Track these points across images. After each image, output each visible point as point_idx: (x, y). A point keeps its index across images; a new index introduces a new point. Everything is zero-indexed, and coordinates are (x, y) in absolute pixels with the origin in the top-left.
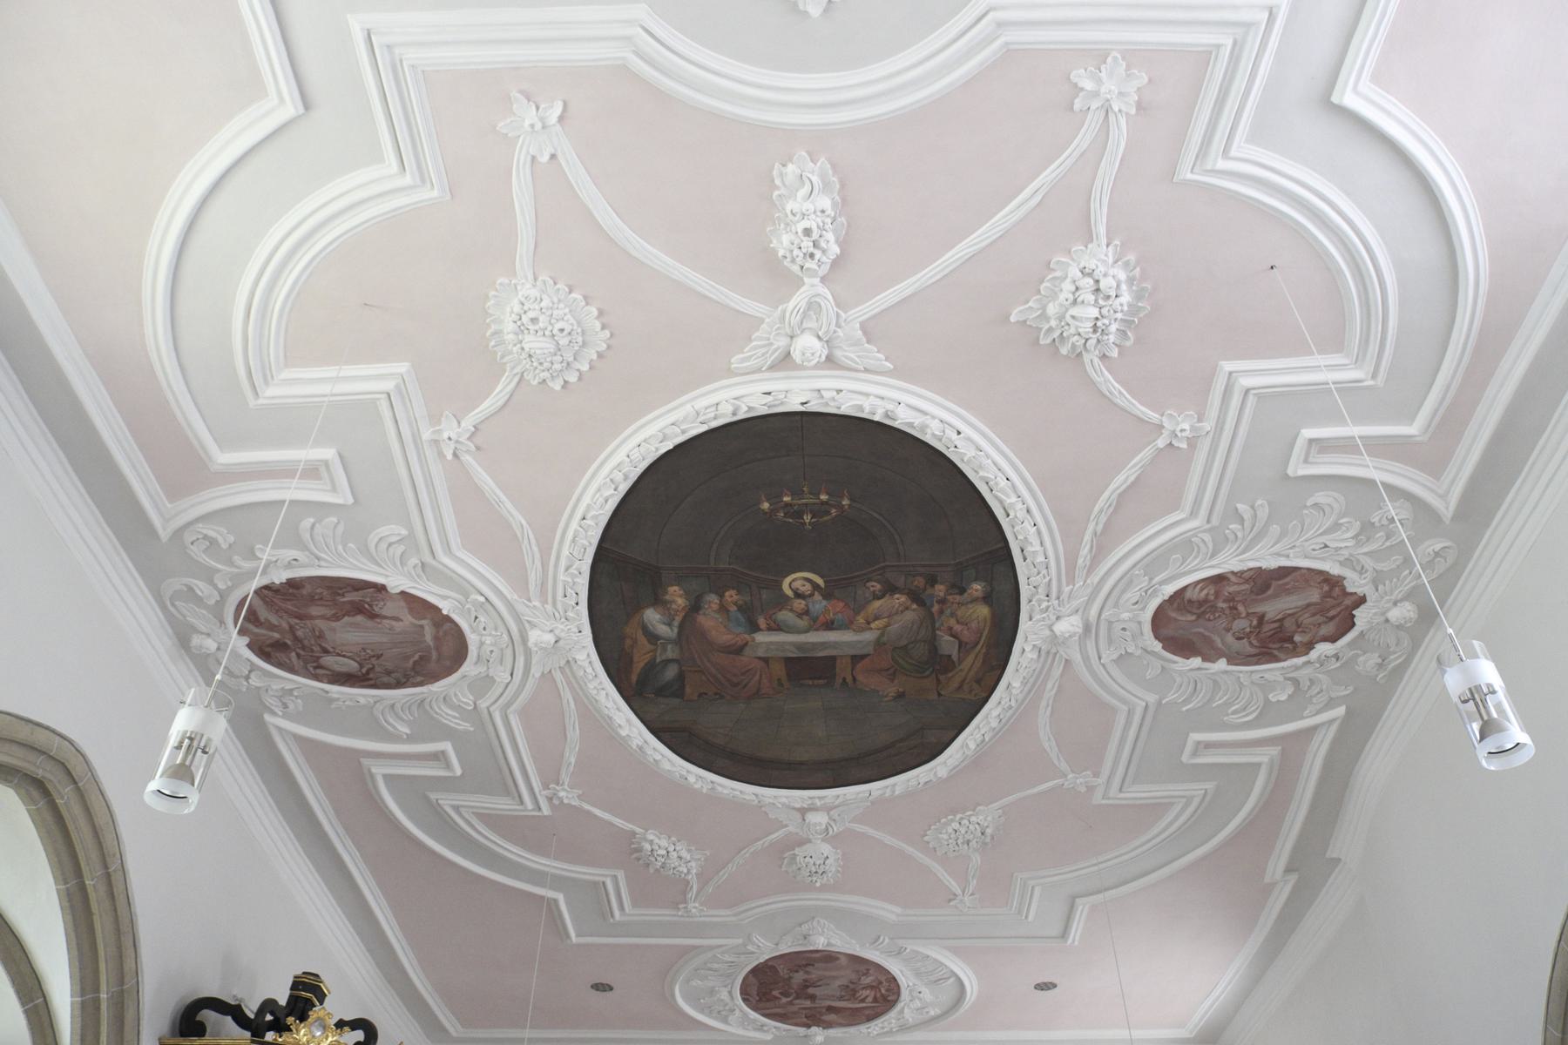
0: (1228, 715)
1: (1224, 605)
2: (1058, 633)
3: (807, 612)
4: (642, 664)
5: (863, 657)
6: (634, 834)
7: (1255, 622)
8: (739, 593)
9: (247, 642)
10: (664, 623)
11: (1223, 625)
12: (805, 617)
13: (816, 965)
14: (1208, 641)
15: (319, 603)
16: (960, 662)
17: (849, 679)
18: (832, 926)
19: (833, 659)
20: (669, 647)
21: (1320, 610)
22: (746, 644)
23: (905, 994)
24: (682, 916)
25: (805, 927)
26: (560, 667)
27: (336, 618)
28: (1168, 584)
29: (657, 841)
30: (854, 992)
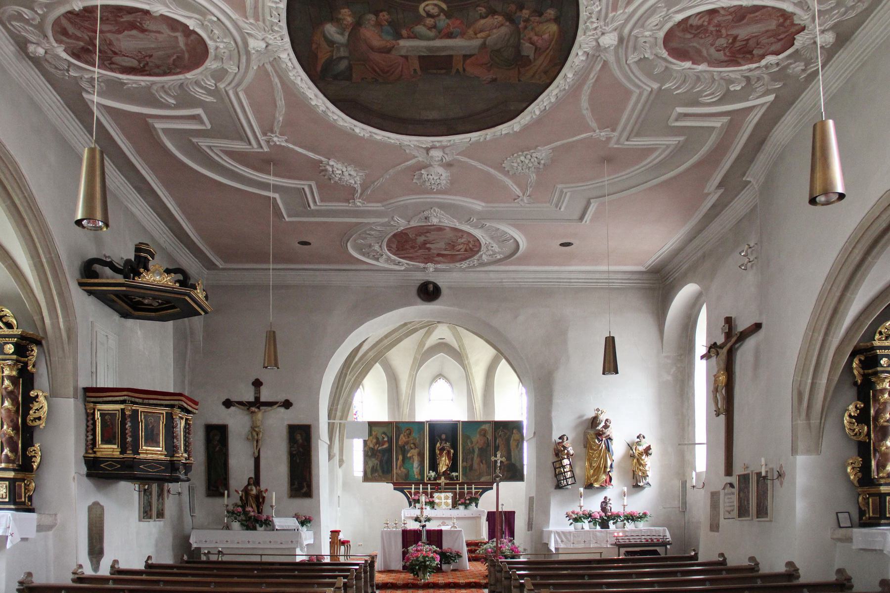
0: (702, 97)
1: (714, 29)
2: (601, 44)
3: (435, 27)
4: (323, 61)
5: (470, 56)
6: (321, 162)
7: (730, 41)
8: (389, 13)
9: (64, 48)
10: (338, 33)
11: (710, 42)
12: (434, 30)
13: (432, 233)
14: (699, 52)
15: (107, 22)
16: (535, 59)
17: (461, 70)
18: (442, 212)
19: (451, 57)
20: (342, 49)
21: (775, 34)
22: (393, 47)
23: (483, 248)
24: (351, 206)
25: (426, 213)
26: (270, 62)
27: (119, 32)
28: (678, 13)
29: (335, 165)
30: (454, 246)
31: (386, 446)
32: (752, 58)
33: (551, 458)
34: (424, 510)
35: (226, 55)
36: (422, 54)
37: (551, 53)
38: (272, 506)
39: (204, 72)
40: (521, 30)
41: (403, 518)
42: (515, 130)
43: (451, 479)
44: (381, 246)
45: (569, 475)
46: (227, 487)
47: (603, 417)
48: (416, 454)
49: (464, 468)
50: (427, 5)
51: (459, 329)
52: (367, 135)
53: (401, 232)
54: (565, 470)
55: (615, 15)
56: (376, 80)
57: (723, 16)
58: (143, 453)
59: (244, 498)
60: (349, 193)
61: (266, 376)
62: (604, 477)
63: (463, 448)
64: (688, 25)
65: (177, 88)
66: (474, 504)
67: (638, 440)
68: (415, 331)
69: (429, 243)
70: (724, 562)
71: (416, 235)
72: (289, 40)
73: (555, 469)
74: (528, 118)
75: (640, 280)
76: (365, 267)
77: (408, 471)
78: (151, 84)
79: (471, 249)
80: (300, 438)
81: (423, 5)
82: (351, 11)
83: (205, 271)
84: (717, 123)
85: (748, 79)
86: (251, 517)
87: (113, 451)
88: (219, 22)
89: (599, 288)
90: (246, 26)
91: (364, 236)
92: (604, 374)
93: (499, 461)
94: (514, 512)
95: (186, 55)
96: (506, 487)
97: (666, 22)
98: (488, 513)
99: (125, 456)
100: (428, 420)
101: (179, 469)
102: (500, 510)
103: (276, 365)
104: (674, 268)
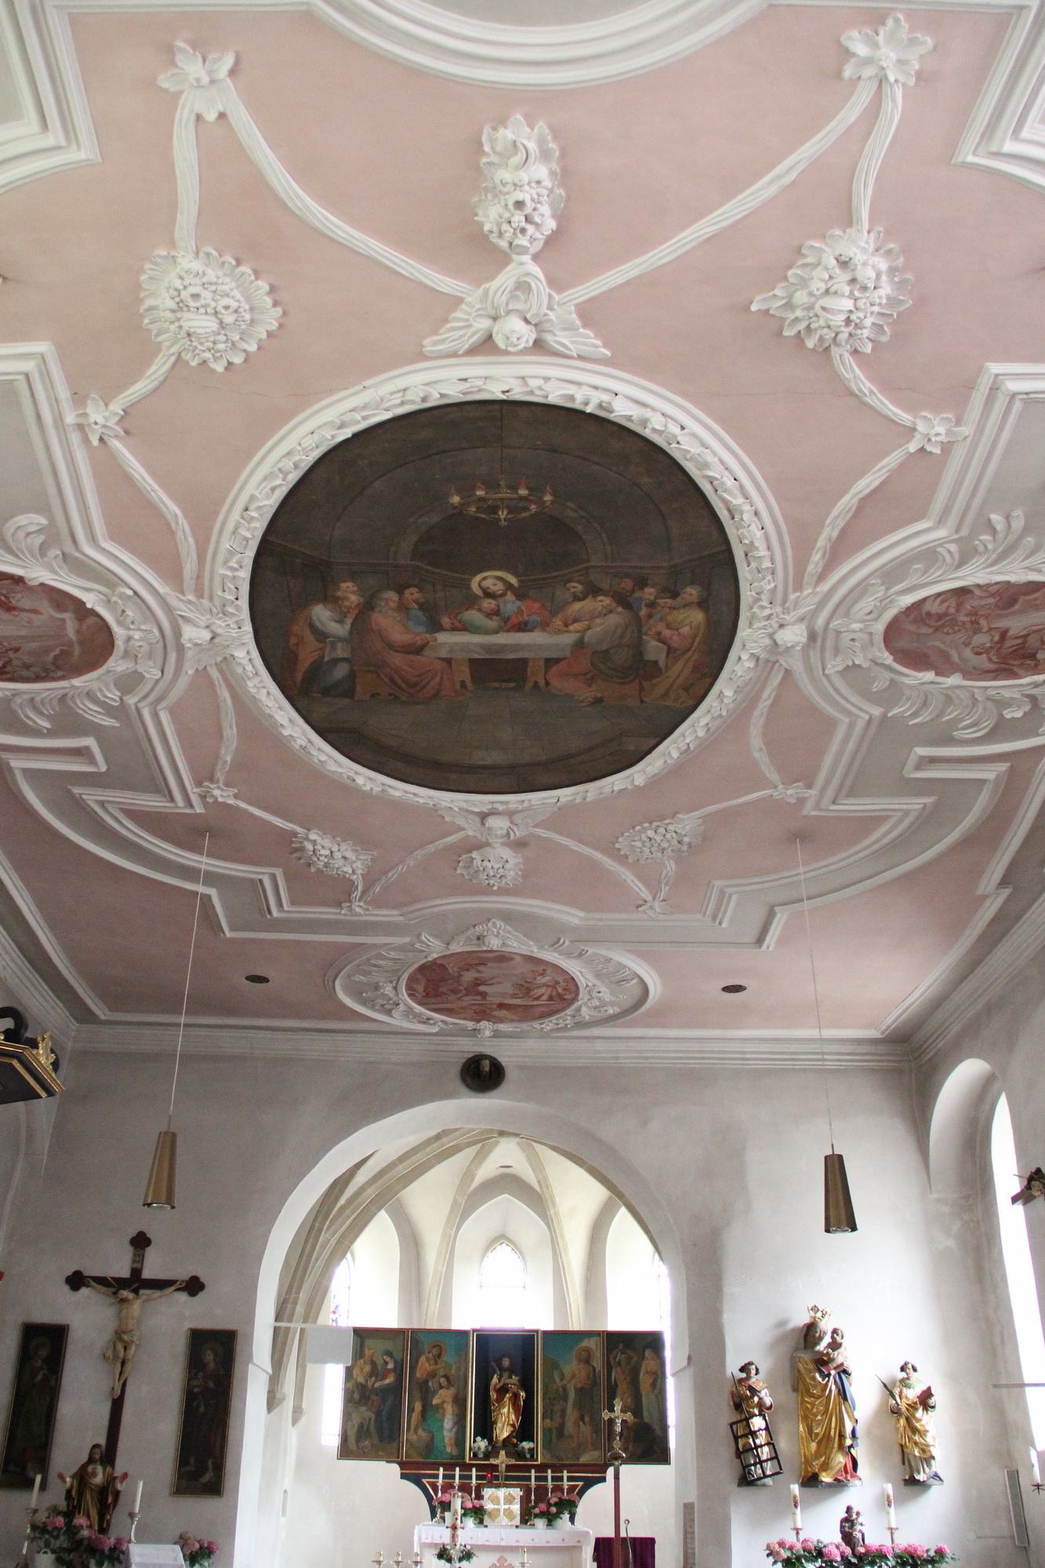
0: (958, 730)
2: (780, 642)
3: (497, 613)
4: (307, 664)
5: (557, 661)
6: (295, 834)
7: (997, 638)
8: (421, 590)
12: (495, 618)
14: (946, 656)
17: (542, 683)
18: (508, 928)
20: (339, 645)
25: (479, 929)
30: (529, 990)
31: (389, 1380)
32: (1036, 665)
33: (728, 1415)
34: (459, 1532)
35: (142, 650)
36: (476, 656)
37: (695, 657)
38: (132, 1515)
39: (103, 678)
41: (416, 1549)
42: (637, 784)
43: (520, 1455)
44: (395, 988)
45: (765, 1452)
46: (43, 1464)
47: (826, 1326)
48: (450, 1399)
49: (547, 1432)
50: (484, 579)
51: (538, 1147)
52: (377, 789)
53: (434, 962)
54: (758, 1442)
55: (798, 597)
56: (396, 698)
57: (981, 598)
60: (341, 890)
61: (157, 1223)
62: (840, 1459)
64: (923, 613)
65: (55, 702)
66: (566, 1516)
67: (903, 1375)
68: (456, 1150)
69: (483, 983)
72: (251, 629)
73: (736, 1438)
74: (659, 764)
75: (871, 1054)
76: (366, 1026)
77: (433, 1438)
78: (13, 695)
79: (560, 996)
80: (212, 1357)
81: (478, 578)
83: (74, 1025)
84: (989, 773)
85: (1033, 699)
86: (82, 1539)
88: (136, 598)
89: (799, 1069)
90: (182, 605)
91: (365, 968)
92: (827, 1230)
93: (619, 1421)
94: (652, 1541)
95: (77, 650)
96: (636, 1478)
97: (886, 608)
98: (598, 1540)
100: (477, 1327)
102: (623, 1534)
103: (170, 1201)
104: (934, 1033)
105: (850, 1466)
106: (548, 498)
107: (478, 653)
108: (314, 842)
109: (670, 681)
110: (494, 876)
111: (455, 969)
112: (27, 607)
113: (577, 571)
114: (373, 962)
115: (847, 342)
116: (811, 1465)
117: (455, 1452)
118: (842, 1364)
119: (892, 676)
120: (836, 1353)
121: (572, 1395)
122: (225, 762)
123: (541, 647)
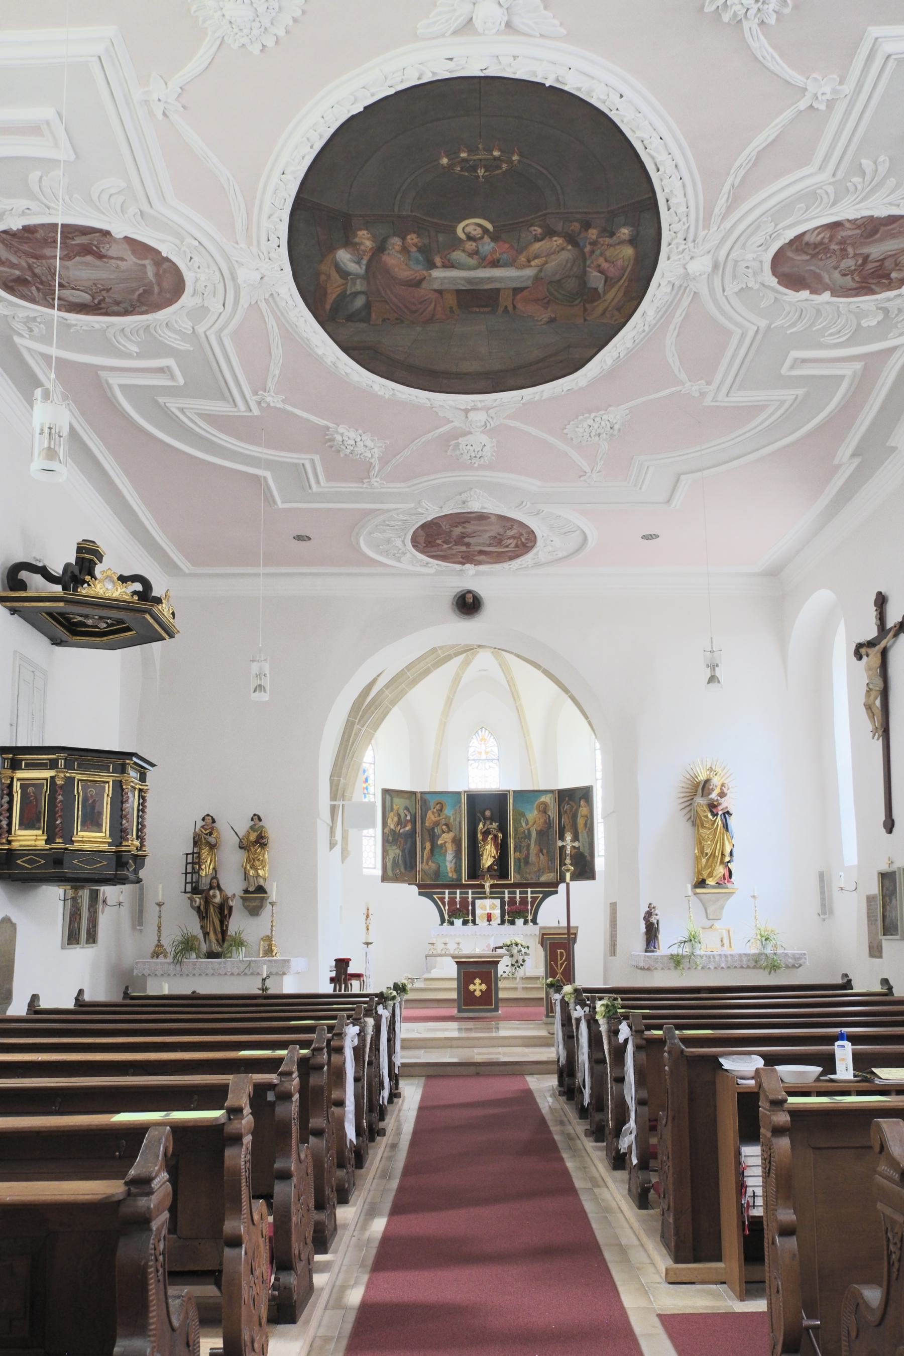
0: (824, 336)
1: (836, 247)
2: (690, 271)
3: (477, 252)
5: (521, 290)
6: (328, 428)
7: (860, 262)
8: (419, 236)
11: (833, 264)
12: (475, 256)
13: (472, 522)
14: (818, 277)
16: (605, 292)
17: (510, 308)
19: (498, 290)
20: (358, 282)
22: (425, 278)
24: (366, 488)
25: (464, 496)
29: (346, 433)
30: (501, 541)
32: (890, 283)
40: (587, 256)
47: (716, 781)
50: (467, 225)
58: (78, 842)
59: (202, 908)
63: (515, 829)
70: (848, 985)
71: (451, 526)
79: (524, 545)
82: (371, 234)
84: (848, 370)
87: (36, 840)
93: (569, 847)
99: (54, 846)
100: (467, 789)
101: (127, 863)
105: (727, 875)
106: (515, 158)
107: (463, 285)
108: (342, 435)
109: (606, 304)
110: (475, 457)
111: (447, 526)
112: (115, 256)
113: (536, 218)
114: (387, 522)
115: (755, 15)
116: (701, 874)
117: (455, 877)
118: (727, 807)
119: (776, 295)
120: (723, 799)
121: (534, 834)
122: (274, 376)
123: (511, 279)
